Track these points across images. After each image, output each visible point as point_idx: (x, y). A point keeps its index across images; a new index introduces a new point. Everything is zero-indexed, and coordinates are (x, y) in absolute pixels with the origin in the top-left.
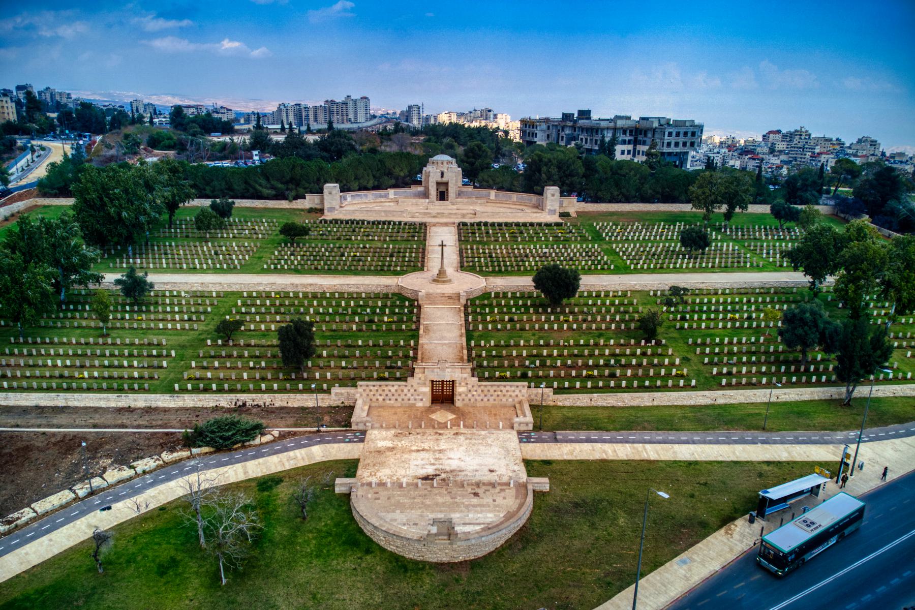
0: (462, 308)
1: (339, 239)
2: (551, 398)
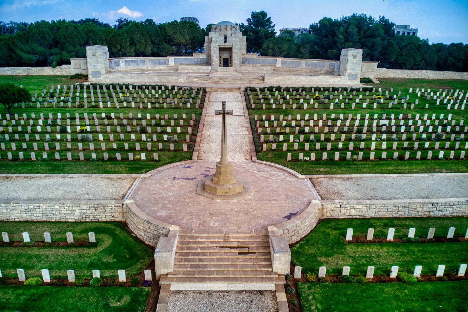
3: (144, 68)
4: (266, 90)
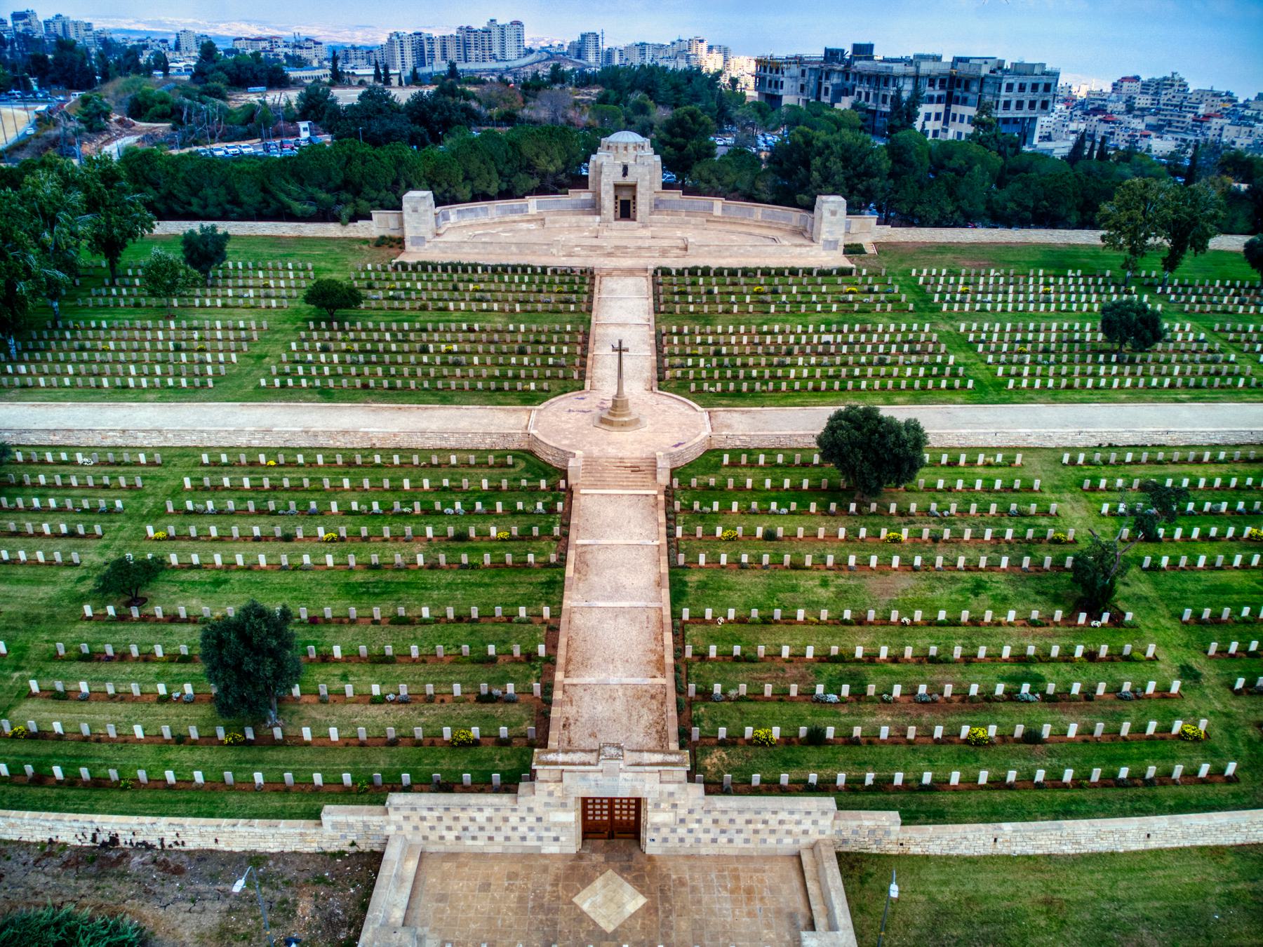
0: (662, 498)
1: (424, 308)
2: (893, 837)
3: (487, 221)
4: (686, 272)
